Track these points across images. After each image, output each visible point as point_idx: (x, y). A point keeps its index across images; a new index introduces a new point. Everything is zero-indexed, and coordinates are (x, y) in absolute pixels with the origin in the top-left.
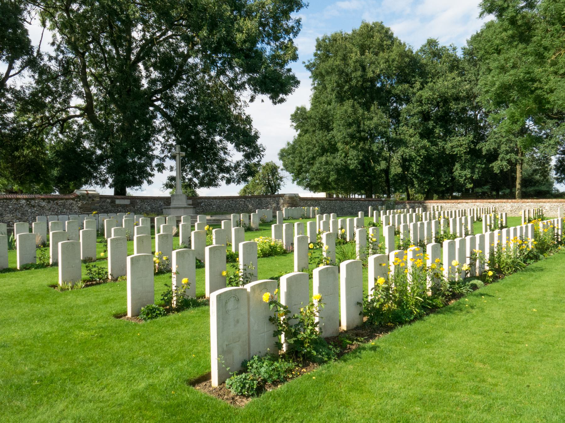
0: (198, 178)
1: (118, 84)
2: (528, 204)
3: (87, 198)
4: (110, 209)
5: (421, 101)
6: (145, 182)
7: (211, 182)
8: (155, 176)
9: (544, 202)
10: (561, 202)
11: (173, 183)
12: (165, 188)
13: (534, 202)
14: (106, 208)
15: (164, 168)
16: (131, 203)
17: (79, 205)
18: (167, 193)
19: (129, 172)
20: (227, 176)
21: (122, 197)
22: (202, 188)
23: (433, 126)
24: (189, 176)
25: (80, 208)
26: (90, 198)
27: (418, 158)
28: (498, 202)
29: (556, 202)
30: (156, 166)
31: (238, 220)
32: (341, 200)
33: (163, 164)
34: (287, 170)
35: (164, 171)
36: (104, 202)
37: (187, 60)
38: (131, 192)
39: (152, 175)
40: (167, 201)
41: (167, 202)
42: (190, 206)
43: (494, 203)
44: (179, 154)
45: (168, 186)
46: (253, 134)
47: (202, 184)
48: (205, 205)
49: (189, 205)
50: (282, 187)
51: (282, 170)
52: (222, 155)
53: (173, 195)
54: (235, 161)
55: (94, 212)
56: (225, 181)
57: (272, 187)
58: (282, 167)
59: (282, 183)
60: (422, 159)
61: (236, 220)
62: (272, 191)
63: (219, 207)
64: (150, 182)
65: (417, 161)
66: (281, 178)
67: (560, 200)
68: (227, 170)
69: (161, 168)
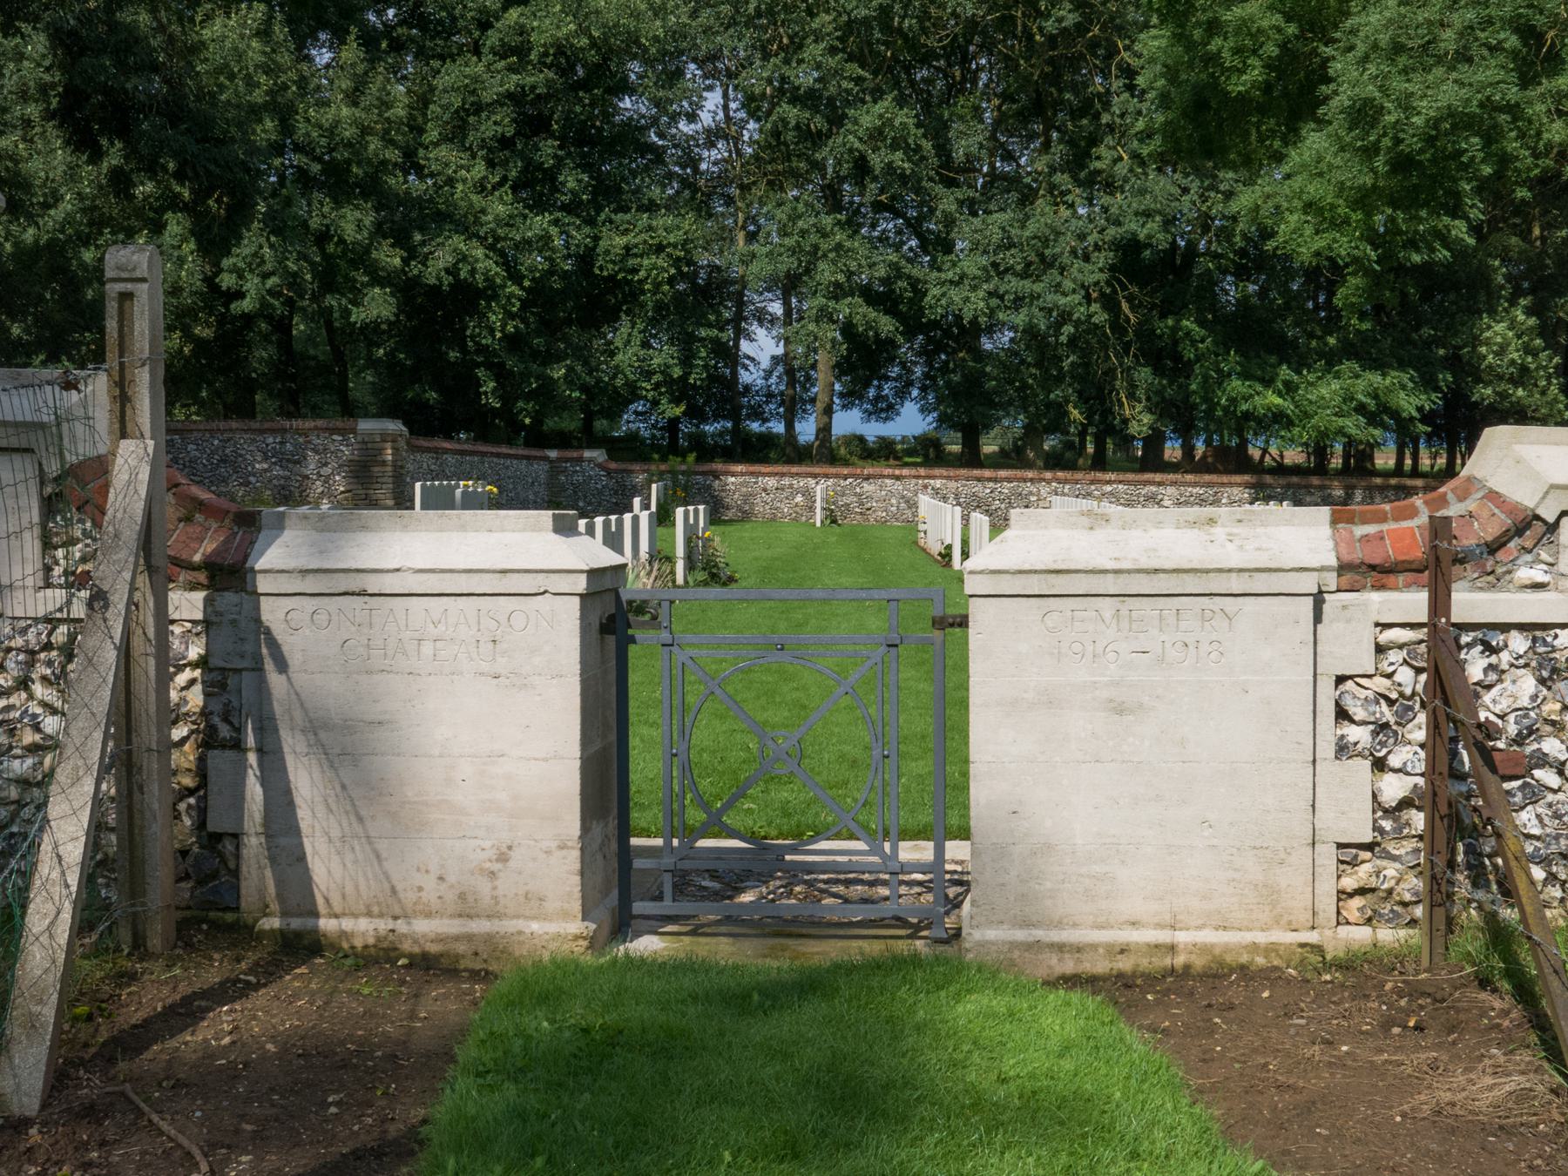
1: (1266, 994)
2: (1108, 488)
5: (522, 51)
9: (1159, 484)
10: (1209, 485)
13: (1128, 483)
23: (555, 156)
27: (512, 289)
28: (1009, 480)
29: (1195, 484)
37: (1495, 172)
43: (995, 480)
60: (528, 290)
65: (509, 297)
67: (1207, 478)
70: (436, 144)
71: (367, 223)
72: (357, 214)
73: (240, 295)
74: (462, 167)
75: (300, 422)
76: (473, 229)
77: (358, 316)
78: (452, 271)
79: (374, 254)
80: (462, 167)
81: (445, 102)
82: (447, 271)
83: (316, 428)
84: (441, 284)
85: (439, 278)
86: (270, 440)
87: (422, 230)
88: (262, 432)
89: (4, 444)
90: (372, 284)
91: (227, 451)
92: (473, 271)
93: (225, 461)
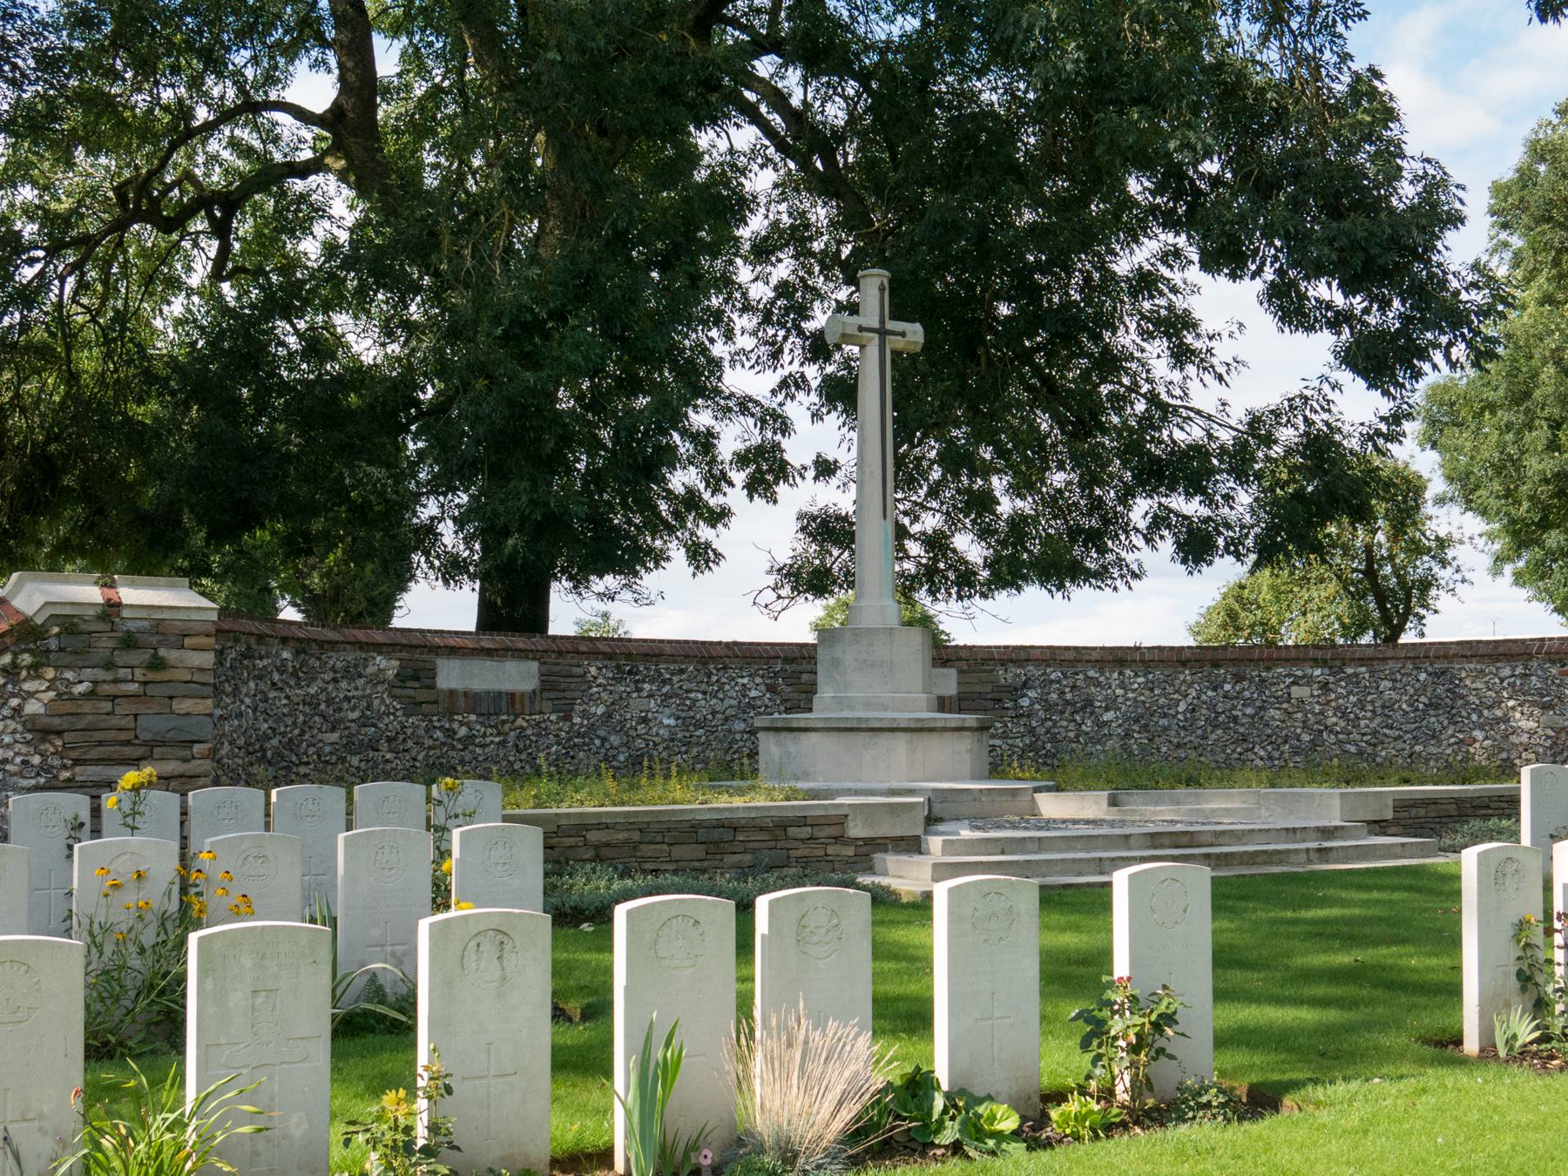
0: (984, 533)
3: (105, 643)
4: (391, 723)
6: (678, 554)
7: (1062, 556)
8: (734, 522)
11: (837, 558)
12: (786, 591)
14: (363, 722)
15: (781, 470)
16: (548, 684)
17: (33, 707)
18: (799, 622)
19: (584, 494)
20: (1192, 507)
21: (520, 642)
22: (1002, 597)
24: (930, 522)
25: (40, 732)
26: (129, 642)
30: (742, 459)
31: (1535, 914)
32: (69, 667)
33: (776, 447)
34: (1469, 505)
35: (782, 489)
36: (352, 672)
38: (567, 611)
39: (718, 517)
40: (788, 673)
41: (793, 679)
42: (953, 718)
44: (882, 332)
45: (809, 580)
46: (1407, 192)
47: (1006, 574)
48: (1049, 707)
49: (943, 704)
50: (1441, 600)
51: (1440, 501)
52: (1161, 367)
53: (822, 631)
54: (1237, 415)
55: (130, 777)
56: (1167, 546)
57: (1382, 597)
58: (1437, 486)
59: (1444, 574)
61: (1512, 914)
62: (1386, 618)
63: (1141, 719)
64: (701, 556)
66: (1443, 544)
68: (1189, 471)
69: (766, 471)
93: (1436, 707)
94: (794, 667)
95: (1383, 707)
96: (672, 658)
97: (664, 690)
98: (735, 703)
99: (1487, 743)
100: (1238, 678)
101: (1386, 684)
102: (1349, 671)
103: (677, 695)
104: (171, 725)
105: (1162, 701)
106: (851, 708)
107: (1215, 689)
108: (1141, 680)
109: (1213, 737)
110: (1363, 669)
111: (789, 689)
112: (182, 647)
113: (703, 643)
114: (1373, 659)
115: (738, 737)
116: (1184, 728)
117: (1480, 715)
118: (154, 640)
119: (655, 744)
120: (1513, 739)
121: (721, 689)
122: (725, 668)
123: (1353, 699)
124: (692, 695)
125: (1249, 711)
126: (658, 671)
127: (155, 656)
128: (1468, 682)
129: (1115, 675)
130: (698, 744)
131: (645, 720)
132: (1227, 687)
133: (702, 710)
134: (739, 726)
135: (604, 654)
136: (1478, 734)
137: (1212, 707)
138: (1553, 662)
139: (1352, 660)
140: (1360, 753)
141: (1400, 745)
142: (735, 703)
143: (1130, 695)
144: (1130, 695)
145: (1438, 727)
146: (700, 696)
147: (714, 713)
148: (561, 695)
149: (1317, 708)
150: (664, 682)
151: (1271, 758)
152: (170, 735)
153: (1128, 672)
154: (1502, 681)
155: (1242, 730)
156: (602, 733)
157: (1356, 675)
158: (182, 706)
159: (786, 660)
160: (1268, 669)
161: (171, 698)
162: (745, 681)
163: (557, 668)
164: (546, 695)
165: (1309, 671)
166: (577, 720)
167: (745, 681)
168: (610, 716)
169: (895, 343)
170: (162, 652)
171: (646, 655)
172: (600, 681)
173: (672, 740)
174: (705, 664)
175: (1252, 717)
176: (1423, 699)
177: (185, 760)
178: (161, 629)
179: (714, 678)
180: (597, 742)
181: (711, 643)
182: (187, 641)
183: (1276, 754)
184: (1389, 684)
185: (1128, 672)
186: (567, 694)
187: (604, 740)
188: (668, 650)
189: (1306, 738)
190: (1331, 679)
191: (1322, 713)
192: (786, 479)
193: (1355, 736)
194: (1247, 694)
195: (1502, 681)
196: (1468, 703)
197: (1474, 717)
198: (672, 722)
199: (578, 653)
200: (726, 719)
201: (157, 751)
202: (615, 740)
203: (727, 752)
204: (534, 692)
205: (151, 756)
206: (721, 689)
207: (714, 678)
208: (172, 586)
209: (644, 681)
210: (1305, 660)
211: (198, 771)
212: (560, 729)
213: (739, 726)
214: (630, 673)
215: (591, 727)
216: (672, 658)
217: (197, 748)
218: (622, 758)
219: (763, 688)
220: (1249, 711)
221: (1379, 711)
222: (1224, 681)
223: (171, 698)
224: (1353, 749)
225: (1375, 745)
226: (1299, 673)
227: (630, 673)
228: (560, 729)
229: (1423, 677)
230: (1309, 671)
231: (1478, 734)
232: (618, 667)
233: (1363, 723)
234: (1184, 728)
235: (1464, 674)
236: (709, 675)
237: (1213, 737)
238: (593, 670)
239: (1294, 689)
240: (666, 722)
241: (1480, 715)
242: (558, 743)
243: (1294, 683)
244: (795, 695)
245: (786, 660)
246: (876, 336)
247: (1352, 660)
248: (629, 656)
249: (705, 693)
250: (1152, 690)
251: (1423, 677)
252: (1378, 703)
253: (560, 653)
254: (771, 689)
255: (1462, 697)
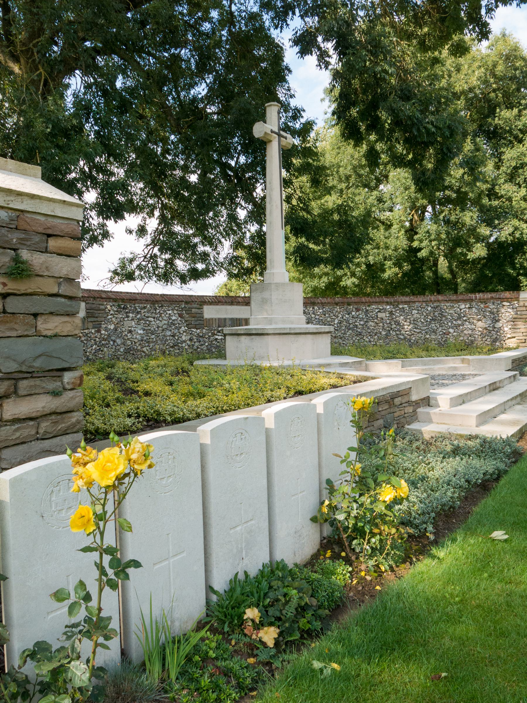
70: (503, 184)
71: (475, 217)
72: (471, 214)
73: (420, 249)
74: (515, 192)
75: (481, 295)
76: (522, 217)
77: (471, 256)
78: (512, 234)
79: (478, 230)
80: (515, 192)
81: (508, 165)
82: (510, 235)
83: (492, 298)
84: (507, 241)
85: (506, 238)
86: (463, 306)
87: (498, 219)
88: (458, 301)
89: (1, 335)
90: (477, 241)
91: (436, 314)
92: (522, 234)
93: (435, 320)
94: (189, 306)
95: (414, 320)
96: (141, 301)
97: (139, 316)
98: (166, 322)
99: (455, 334)
100: (358, 310)
101: (414, 312)
102: (401, 306)
103: (143, 319)
104: (40, 350)
105: (329, 319)
106: (276, 323)
107: (349, 314)
108: (321, 311)
109: (348, 333)
110: (406, 306)
111: (187, 316)
112: (46, 251)
113: (152, 294)
114: (410, 302)
115: (168, 338)
116: (337, 330)
117: (452, 323)
118: (14, 238)
119: (135, 343)
120: (465, 332)
121: (161, 316)
122: (162, 306)
123: (402, 317)
124: (150, 319)
125: (362, 323)
126: (135, 307)
127: (17, 260)
128: (447, 311)
129: (311, 309)
130: (153, 342)
131: (130, 332)
132: (353, 313)
133: (153, 327)
134: (168, 333)
135: (113, 299)
136: (451, 330)
137: (347, 321)
138: (482, 302)
139: (402, 302)
140: (405, 338)
141: (420, 335)
142: (166, 322)
143: (317, 317)
144: (317, 317)
145: (435, 328)
146: (152, 319)
147: (158, 327)
148: (96, 319)
149: (388, 321)
150: (138, 313)
151: (370, 341)
152: (37, 364)
153: (316, 308)
154: (461, 310)
155: (359, 330)
156: (113, 338)
157: (403, 308)
158: (50, 325)
159: (187, 303)
160: (369, 306)
161: (35, 315)
162: (170, 312)
163: (94, 306)
164: (90, 320)
165: (385, 307)
166: (103, 332)
167: (170, 312)
168: (116, 330)
169: (284, 142)
170: (25, 254)
171: (130, 300)
172: (112, 312)
173: (142, 340)
174: (154, 304)
175: (363, 325)
176: (429, 317)
177: (56, 394)
178: (22, 225)
179: (158, 311)
180: (111, 343)
181: (155, 295)
182: (52, 243)
183: (372, 340)
184: (416, 312)
185: (316, 308)
186: (99, 319)
187: (114, 341)
188: (138, 297)
189: (384, 333)
190: (394, 310)
191: (390, 323)
192: (107, 238)
193: (403, 332)
194: (361, 316)
195: (461, 310)
196: (447, 319)
197: (450, 324)
198: (141, 332)
199: (102, 298)
200: (163, 330)
201: (23, 385)
202: (119, 341)
203: (164, 345)
204: (84, 318)
205: (15, 392)
206: (161, 316)
207: (158, 311)
208: (24, 173)
209: (129, 313)
210: (383, 302)
211: (71, 405)
212: (96, 337)
213: (168, 333)
214: (124, 308)
215: (109, 336)
216: (141, 301)
217: (68, 377)
218: (122, 350)
219: (177, 315)
220: (362, 323)
221: (412, 322)
222: (352, 311)
223: (35, 315)
224: (402, 337)
225: (410, 336)
226: (381, 308)
227: (124, 308)
228: (96, 337)
229: (429, 309)
230: (385, 307)
231: (451, 330)
232: (119, 306)
233: (406, 327)
234: (337, 330)
235: (445, 307)
236: (156, 309)
237: (348, 333)
238: (109, 307)
239: (379, 314)
240: (140, 332)
241: (452, 323)
242: (96, 344)
243: (379, 312)
244: (190, 319)
245: (187, 303)
246: (277, 136)
247: (402, 302)
248: (123, 300)
249: (154, 318)
250: (325, 315)
251: (429, 309)
252: (412, 319)
253: (94, 298)
254: (180, 316)
255: (444, 316)
